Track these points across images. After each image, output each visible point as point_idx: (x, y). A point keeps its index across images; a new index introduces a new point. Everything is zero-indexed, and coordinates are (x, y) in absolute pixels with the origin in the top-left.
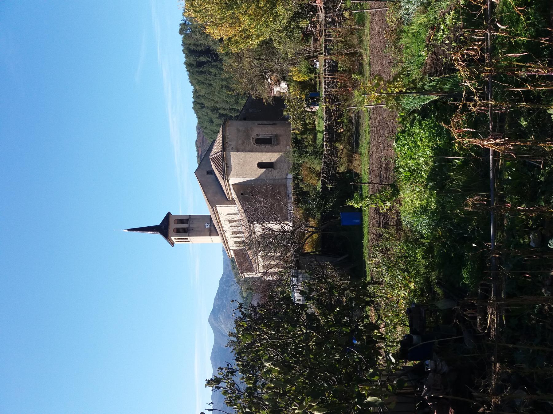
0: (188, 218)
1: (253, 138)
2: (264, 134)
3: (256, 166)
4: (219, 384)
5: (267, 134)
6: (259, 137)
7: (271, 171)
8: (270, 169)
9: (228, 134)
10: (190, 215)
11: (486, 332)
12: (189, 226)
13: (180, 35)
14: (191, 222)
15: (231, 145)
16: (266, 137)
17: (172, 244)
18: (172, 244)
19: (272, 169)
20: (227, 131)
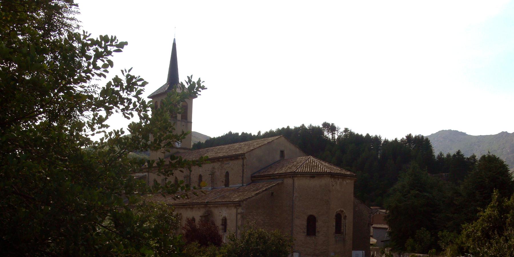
0: (189, 120)
1: (342, 211)
2: (347, 226)
3: (311, 214)
4: (132, 102)
5: (347, 229)
6: (343, 218)
7: (304, 232)
8: (305, 230)
9: (347, 181)
10: (191, 123)
11: (108, 242)
12: (179, 121)
13: (322, 123)
14: (183, 123)
15: (336, 183)
16: (342, 227)
17: (190, 100)
18: (190, 100)
19: (306, 234)
20: (350, 181)
